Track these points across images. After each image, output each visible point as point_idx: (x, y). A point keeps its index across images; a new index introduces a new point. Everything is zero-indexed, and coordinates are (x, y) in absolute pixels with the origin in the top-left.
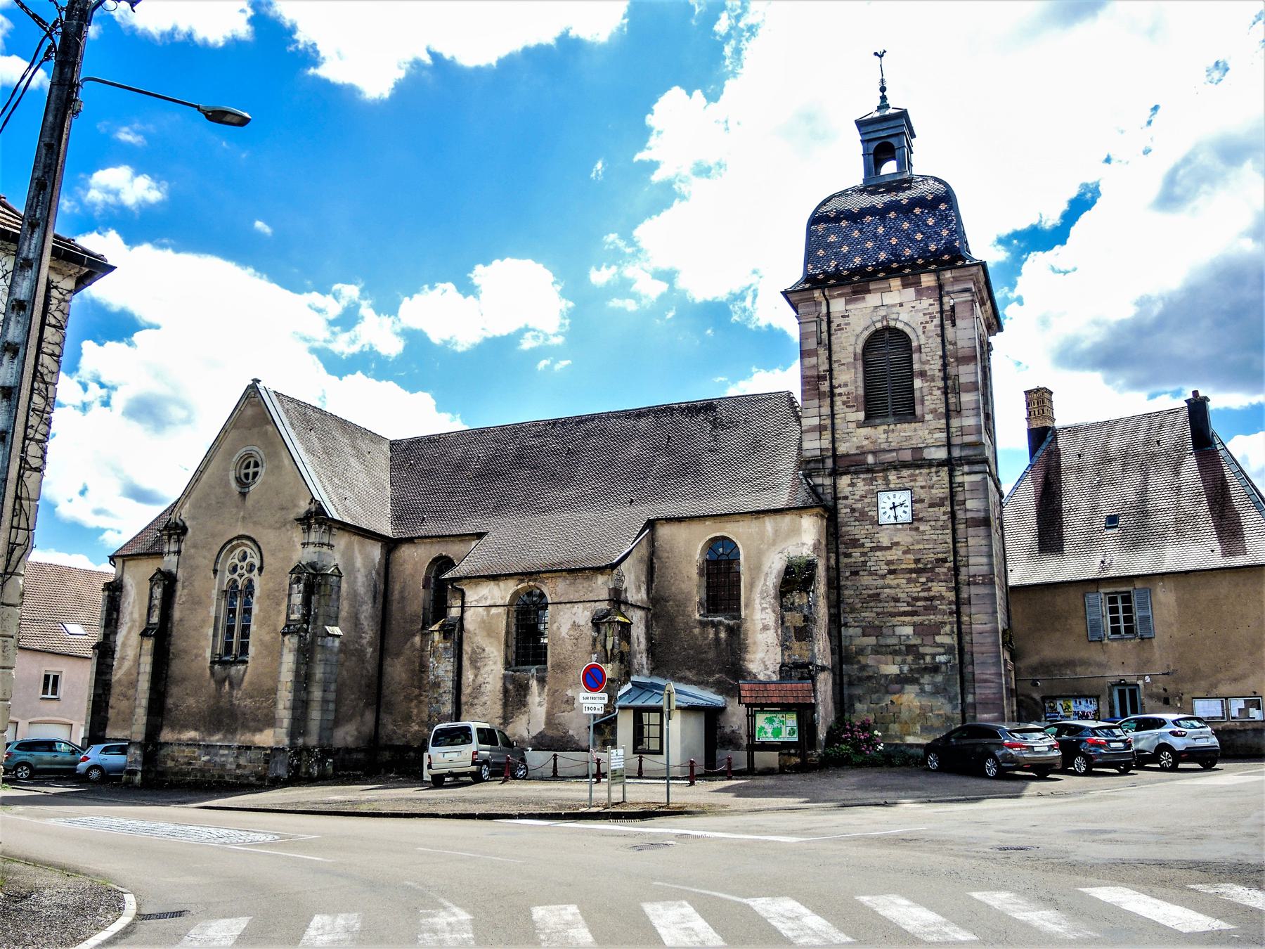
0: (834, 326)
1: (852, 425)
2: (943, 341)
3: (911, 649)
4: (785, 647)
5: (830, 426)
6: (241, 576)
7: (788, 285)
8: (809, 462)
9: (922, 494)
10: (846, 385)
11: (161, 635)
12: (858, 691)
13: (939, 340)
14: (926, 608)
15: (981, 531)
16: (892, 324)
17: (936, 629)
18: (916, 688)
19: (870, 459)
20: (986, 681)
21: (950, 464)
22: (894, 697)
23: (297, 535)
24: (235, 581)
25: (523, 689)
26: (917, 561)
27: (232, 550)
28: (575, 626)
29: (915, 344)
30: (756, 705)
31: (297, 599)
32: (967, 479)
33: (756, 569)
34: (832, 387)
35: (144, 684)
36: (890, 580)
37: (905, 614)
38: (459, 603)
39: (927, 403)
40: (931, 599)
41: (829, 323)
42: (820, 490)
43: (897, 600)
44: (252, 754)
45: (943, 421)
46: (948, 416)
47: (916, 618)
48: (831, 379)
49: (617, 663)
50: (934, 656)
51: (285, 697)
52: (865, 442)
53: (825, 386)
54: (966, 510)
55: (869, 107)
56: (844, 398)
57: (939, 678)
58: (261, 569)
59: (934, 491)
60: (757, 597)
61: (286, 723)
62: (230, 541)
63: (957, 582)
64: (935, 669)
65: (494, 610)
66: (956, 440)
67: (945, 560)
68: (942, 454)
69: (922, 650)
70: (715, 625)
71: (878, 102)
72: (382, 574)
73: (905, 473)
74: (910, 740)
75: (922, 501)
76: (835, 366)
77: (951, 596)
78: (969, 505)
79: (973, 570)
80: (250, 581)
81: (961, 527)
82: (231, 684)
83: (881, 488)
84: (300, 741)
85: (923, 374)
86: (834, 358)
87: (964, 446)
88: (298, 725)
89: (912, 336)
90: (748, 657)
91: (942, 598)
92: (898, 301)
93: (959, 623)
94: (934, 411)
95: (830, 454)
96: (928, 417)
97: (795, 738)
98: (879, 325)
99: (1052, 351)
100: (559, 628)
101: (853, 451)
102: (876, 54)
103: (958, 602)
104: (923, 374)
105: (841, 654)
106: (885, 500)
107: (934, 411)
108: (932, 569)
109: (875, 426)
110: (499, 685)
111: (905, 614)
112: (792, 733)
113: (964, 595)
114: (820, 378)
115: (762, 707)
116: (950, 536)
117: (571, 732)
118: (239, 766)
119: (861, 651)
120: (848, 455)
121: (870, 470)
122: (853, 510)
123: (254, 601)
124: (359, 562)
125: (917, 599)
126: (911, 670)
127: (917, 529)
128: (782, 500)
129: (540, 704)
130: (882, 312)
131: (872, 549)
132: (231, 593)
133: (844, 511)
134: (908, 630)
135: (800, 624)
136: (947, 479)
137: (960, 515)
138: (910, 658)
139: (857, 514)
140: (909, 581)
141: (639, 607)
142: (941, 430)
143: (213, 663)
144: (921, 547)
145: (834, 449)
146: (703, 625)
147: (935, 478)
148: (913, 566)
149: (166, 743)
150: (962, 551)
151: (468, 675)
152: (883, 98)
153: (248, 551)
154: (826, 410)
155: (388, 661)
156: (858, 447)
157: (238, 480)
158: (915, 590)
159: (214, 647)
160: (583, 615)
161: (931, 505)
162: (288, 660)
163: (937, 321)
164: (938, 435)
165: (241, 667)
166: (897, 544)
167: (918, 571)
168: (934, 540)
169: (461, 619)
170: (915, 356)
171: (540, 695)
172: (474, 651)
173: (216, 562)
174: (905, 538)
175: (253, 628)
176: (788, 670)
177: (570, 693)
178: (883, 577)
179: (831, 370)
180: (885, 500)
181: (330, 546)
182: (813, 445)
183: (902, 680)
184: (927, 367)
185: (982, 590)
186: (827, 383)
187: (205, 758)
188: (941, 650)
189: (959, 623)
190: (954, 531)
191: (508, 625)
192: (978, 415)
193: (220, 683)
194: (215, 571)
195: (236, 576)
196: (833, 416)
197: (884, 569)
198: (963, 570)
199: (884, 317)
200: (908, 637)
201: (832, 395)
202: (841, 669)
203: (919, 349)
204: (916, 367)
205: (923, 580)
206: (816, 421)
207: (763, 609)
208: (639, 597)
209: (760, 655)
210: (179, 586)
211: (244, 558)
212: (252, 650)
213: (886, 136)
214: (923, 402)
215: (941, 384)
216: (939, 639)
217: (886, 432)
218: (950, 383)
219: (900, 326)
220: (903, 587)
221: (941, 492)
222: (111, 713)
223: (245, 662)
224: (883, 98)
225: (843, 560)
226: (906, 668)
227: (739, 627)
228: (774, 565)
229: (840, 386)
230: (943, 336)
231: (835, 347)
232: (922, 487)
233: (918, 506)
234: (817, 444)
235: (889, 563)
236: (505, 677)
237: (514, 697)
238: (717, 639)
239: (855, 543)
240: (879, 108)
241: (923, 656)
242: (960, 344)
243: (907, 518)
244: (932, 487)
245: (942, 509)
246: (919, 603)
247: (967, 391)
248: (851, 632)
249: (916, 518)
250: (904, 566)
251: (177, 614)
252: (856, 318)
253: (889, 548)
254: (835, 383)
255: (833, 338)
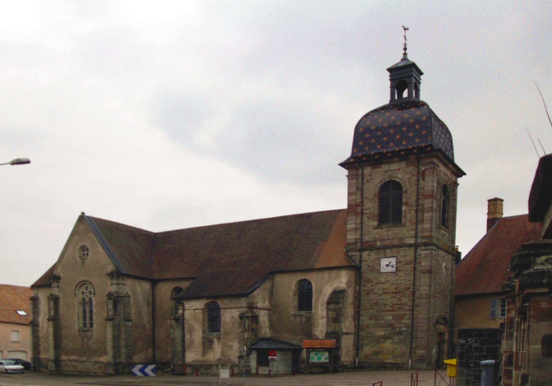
0: (365, 180)
1: (371, 228)
2: (418, 188)
3: (391, 325)
4: (328, 326)
5: (360, 228)
6: (87, 296)
7: (343, 159)
8: (349, 244)
9: (402, 259)
10: (369, 209)
11: (55, 319)
12: (365, 342)
13: (416, 187)
14: (399, 308)
15: (427, 275)
16: (394, 179)
17: (402, 317)
18: (391, 341)
19: (379, 244)
20: (421, 338)
21: (416, 246)
22: (381, 344)
23: (108, 281)
24: (84, 299)
25: (211, 342)
26: (396, 288)
27: (81, 286)
28: (232, 317)
29: (404, 189)
30: (310, 348)
31: (111, 306)
32: (423, 252)
33: (320, 293)
34: (362, 210)
35: (51, 338)
36: (384, 297)
37: (389, 311)
38: (182, 308)
39: (407, 217)
40: (402, 304)
41: (363, 178)
42: (354, 258)
43: (386, 305)
44: (98, 365)
45: (414, 226)
46: (417, 223)
47: (394, 313)
48: (362, 206)
49: (250, 332)
50: (400, 328)
51: (109, 344)
52: (377, 236)
53: (359, 209)
54: (421, 266)
55: (395, 59)
56: (368, 215)
57: (402, 337)
58: (94, 294)
59: (407, 258)
60: (320, 305)
61: (111, 353)
62: (80, 282)
63: (414, 298)
64: (400, 333)
65: (197, 311)
66: (420, 235)
67: (409, 288)
68: (412, 241)
69: (395, 325)
70: (301, 316)
71: (401, 56)
72: (151, 294)
73: (394, 250)
74: (387, 361)
75: (401, 262)
76: (365, 200)
77: (411, 303)
78: (423, 264)
79: (421, 292)
80: (90, 298)
81: (418, 274)
82: (88, 338)
83: (382, 256)
84: (118, 361)
85: (407, 204)
86: (364, 196)
87: (423, 237)
88: (116, 354)
89: (403, 185)
90: (314, 329)
91: (406, 304)
92: (397, 168)
93: (413, 314)
94: (410, 221)
95: (359, 241)
96: (408, 224)
97: (327, 361)
98: (387, 180)
99: (489, 184)
100: (225, 318)
101: (371, 240)
102: (408, 29)
103: (413, 306)
104: (407, 204)
105: (358, 327)
106: (384, 262)
107: (410, 221)
108: (403, 292)
109: (382, 228)
110: (201, 340)
111: (389, 311)
112: (326, 359)
113: (416, 303)
114: (357, 205)
115: (314, 349)
116: (413, 278)
117: (232, 358)
118: (95, 369)
119: (368, 326)
120: (368, 241)
121: (378, 249)
122: (369, 266)
123: (93, 306)
124: (139, 290)
125: (394, 305)
126: (390, 334)
127: (398, 275)
128: (335, 263)
129: (218, 348)
130: (389, 173)
131: (377, 283)
132: (84, 303)
133: (364, 266)
134: (390, 317)
135: (335, 316)
136: (413, 252)
137: (419, 268)
138: (389, 329)
139: (371, 268)
140: (392, 297)
141: (260, 309)
142: (413, 230)
143: (79, 331)
144: (399, 282)
145: (362, 239)
146: (295, 316)
147: (408, 252)
148: (394, 290)
149: (64, 360)
150: (417, 284)
151: (188, 337)
152: (405, 54)
153: (88, 286)
154: (359, 221)
155: (156, 330)
156: (373, 238)
157: (80, 257)
158: (394, 301)
159: (78, 326)
160: (236, 313)
161: (405, 264)
162: (109, 331)
163: (415, 178)
164: (411, 232)
165: (91, 333)
166: (387, 281)
167: (396, 293)
168: (405, 279)
169: (183, 314)
170: (404, 195)
171: (218, 344)
172: (189, 327)
173: (75, 291)
174: (391, 278)
175: (94, 317)
176: (329, 335)
177: (231, 343)
178: (380, 295)
179: (362, 202)
180: (384, 262)
181: (124, 285)
182: (351, 237)
183: (385, 338)
184: (409, 200)
185: (425, 301)
186: (360, 208)
187: (81, 366)
188: (404, 325)
189: (413, 314)
190: (415, 275)
191: (203, 317)
192: (431, 223)
193: (83, 338)
194: (75, 295)
195: (84, 296)
196: (362, 223)
197: (381, 292)
198: (417, 292)
199: (390, 176)
200: (390, 320)
201: (362, 213)
202: (359, 333)
203: (406, 192)
204: (404, 200)
205: (398, 296)
206: (354, 226)
207: (322, 310)
208: (265, 305)
209: (319, 328)
210: (61, 300)
211: (87, 288)
212: (94, 325)
213: (405, 76)
214: (405, 217)
215: (415, 208)
216: (403, 321)
217: (387, 231)
218: (419, 208)
219: (397, 180)
220: (389, 300)
221: (411, 258)
222: (41, 348)
223: (92, 331)
224: (405, 54)
225: (363, 288)
226: (387, 333)
227: (311, 317)
228: (328, 291)
229: (366, 209)
230: (418, 185)
231: (365, 191)
232: (402, 256)
233: (399, 264)
234: (353, 237)
235: (383, 289)
236: (203, 337)
237: (207, 344)
238: (301, 321)
239: (369, 281)
240: (402, 60)
241: (395, 328)
242: (426, 189)
243: (394, 270)
244: (406, 256)
245: (410, 266)
246: (396, 306)
247: (428, 211)
248: (365, 319)
249: (397, 269)
250: (391, 291)
251: (61, 310)
252: (376, 177)
253: (383, 283)
254: (364, 207)
255: (364, 187)
